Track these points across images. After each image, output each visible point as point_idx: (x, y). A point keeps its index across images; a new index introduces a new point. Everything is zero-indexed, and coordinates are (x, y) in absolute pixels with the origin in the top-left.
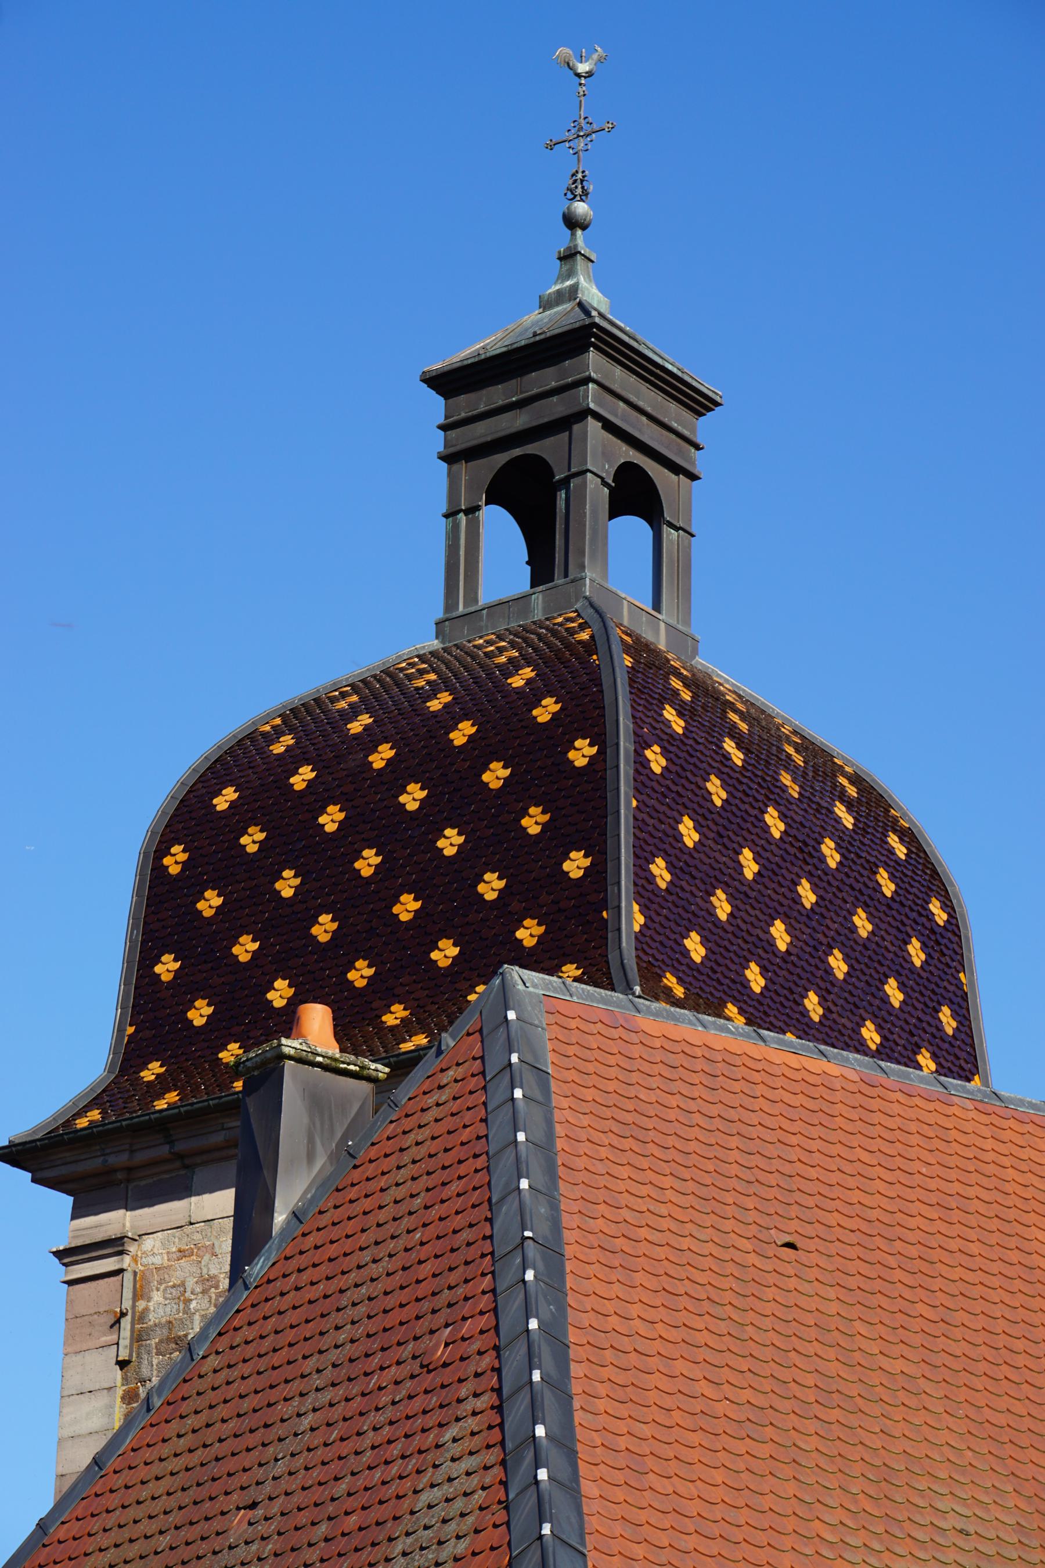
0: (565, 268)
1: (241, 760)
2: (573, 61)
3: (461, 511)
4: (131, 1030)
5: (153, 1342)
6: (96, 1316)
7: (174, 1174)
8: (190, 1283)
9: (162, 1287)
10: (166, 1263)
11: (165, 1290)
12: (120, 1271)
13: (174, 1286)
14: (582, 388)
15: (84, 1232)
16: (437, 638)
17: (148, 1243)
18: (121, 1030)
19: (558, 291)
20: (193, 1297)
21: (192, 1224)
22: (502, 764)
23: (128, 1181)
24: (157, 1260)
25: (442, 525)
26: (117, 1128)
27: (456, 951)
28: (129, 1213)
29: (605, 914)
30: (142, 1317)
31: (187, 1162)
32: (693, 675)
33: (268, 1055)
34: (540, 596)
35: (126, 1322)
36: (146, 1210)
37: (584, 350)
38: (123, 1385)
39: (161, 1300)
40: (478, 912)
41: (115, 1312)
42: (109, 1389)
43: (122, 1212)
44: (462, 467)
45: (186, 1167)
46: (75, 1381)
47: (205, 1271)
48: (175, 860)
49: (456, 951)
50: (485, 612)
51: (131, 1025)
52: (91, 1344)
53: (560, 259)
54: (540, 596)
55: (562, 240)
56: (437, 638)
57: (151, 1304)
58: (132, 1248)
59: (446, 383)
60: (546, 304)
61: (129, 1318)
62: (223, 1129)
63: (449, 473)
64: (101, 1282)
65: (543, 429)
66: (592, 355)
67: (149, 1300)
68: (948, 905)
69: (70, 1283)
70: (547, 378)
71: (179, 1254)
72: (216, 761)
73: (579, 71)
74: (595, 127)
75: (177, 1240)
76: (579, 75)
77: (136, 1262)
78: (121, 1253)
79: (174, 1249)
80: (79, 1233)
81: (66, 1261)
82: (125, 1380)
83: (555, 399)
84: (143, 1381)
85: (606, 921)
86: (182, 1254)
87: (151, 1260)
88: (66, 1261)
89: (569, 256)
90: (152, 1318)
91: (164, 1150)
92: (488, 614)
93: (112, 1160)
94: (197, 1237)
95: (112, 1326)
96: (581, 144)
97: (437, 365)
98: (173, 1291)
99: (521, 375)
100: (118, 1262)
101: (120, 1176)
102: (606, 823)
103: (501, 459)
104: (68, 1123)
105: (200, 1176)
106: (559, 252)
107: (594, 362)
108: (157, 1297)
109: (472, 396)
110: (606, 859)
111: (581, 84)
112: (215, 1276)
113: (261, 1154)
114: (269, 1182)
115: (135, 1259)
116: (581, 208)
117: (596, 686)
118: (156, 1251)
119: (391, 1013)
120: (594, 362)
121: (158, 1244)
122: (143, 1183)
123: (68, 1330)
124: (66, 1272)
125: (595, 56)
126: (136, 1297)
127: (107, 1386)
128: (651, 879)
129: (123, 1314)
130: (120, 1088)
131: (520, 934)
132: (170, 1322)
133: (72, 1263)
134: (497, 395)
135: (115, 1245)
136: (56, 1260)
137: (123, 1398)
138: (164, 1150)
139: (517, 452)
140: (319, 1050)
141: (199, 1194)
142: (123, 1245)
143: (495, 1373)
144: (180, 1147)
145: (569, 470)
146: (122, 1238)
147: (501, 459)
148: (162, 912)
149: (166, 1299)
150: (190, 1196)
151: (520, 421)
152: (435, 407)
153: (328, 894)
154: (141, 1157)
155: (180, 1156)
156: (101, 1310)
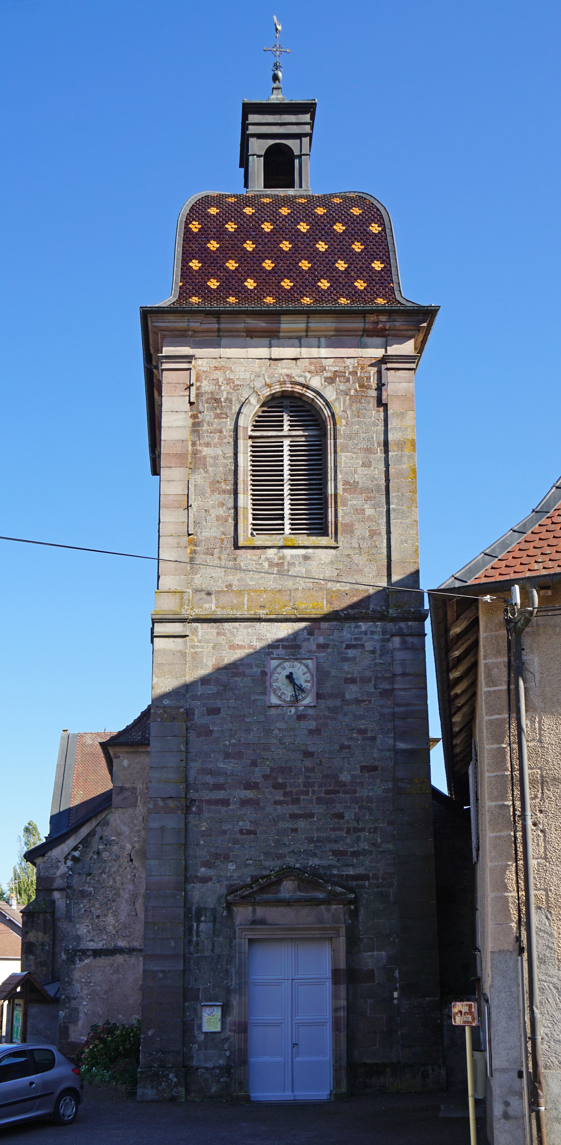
5: (204, 398)
8: (221, 380)
12: (190, 369)
13: (213, 379)
17: (200, 362)
32: (476, 863)
35: (193, 389)
58: (193, 361)
64: (179, 372)
67: (201, 383)
68: (382, 224)
78: (190, 362)
87: (201, 368)
90: (203, 390)
94: (223, 364)
101: (190, 333)
105: (224, 341)
108: (205, 382)
112: (232, 379)
122: (197, 339)
128: (210, 206)
135: (189, 358)
143: (383, 402)
144: (223, 326)
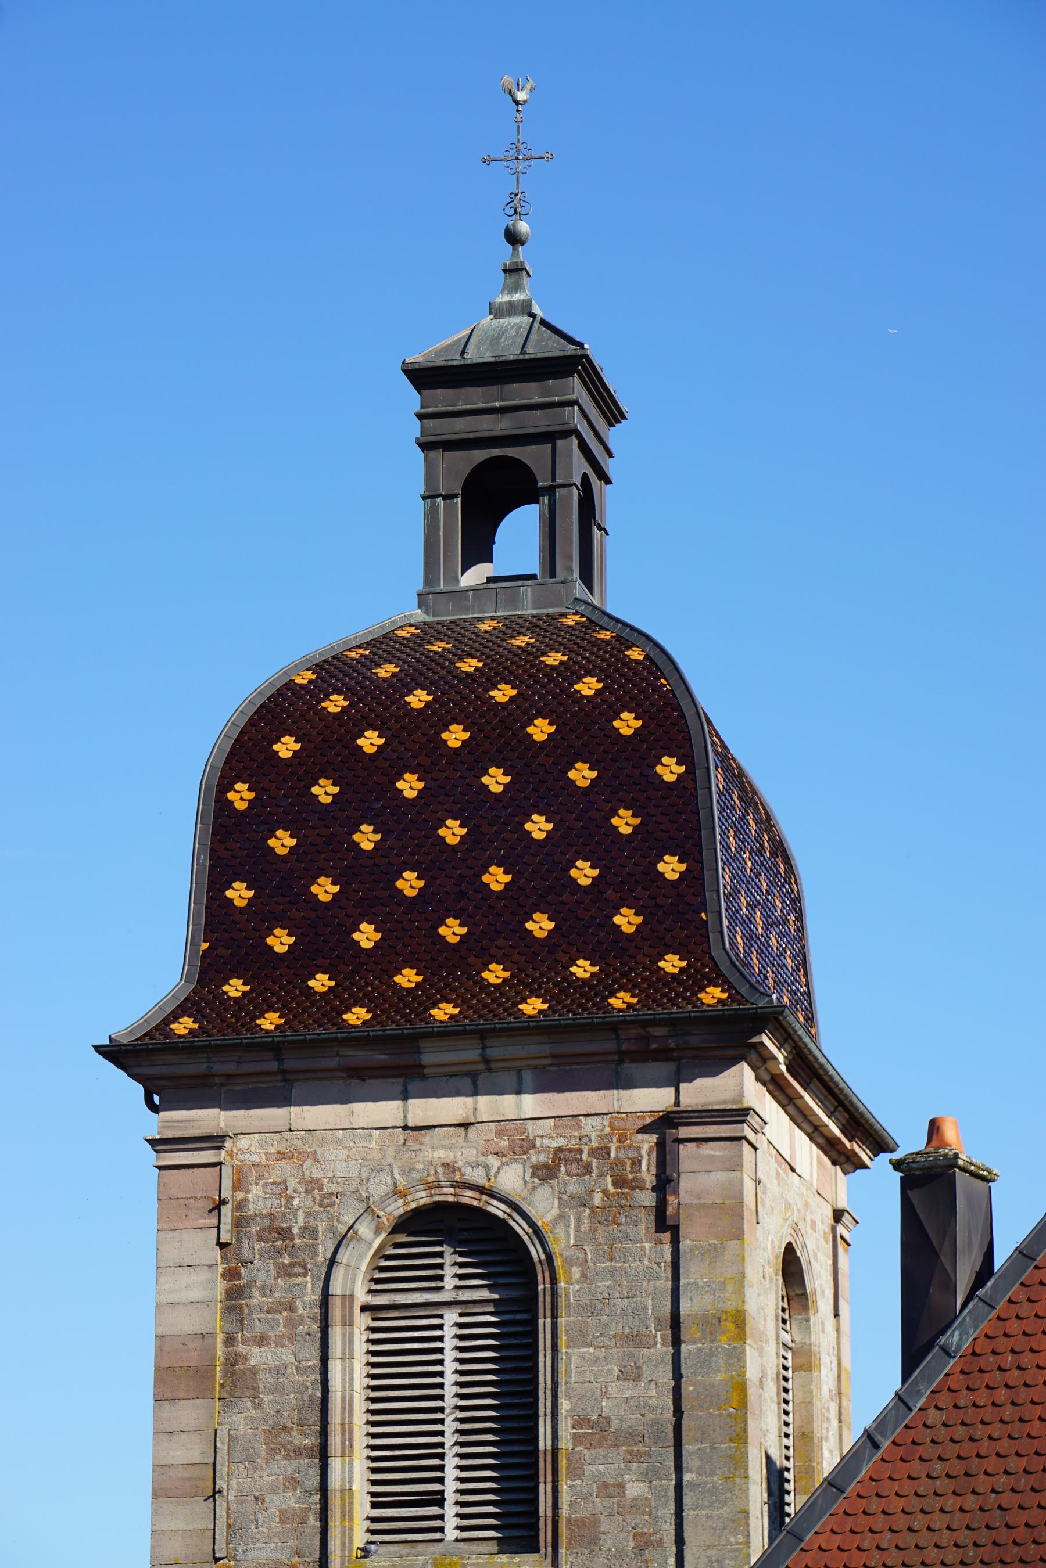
0: (511, 280)
1: (281, 708)
2: (514, 89)
3: (441, 495)
4: (205, 946)
6: (192, 1201)
7: (270, 1085)
8: (292, 1183)
9: (262, 1182)
10: (264, 1162)
11: (265, 1186)
13: (274, 1183)
14: (567, 409)
15: (180, 1124)
16: (419, 607)
17: (244, 1142)
18: (194, 945)
19: (510, 303)
20: (295, 1195)
21: (291, 1130)
22: (588, 765)
23: (222, 1085)
24: (255, 1159)
25: (419, 507)
26: (238, 1044)
27: (551, 925)
28: (222, 1112)
29: (703, 915)
30: (240, 1206)
31: (288, 1076)
33: (940, 1163)
34: (529, 589)
35: (227, 1211)
36: (242, 1112)
37: (570, 374)
38: (222, 1263)
39: (261, 1193)
40: (572, 894)
41: (214, 1200)
42: (211, 1266)
43: (216, 1111)
44: (436, 455)
45: (285, 1080)
46: (172, 1254)
47: (307, 1173)
48: (241, 796)
49: (551, 925)
50: (471, 593)
51: (204, 941)
52: (187, 1224)
53: (505, 271)
54: (529, 589)
55: (505, 253)
56: (419, 607)
57: (250, 1196)
59: (421, 377)
60: (497, 311)
61: (230, 1206)
62: (338, 1055)
63: (426, 459)
65: (510, 433)
66: (576, 380)
67: (248, 1192)
69: (160, 1168)
70: (529, 392)
71: (277, 1156)
72: (261, 706)
73: (519, 99)
74: (534, 154)
75: (275, 1143)
76: (517, 103)
77: (231, 1156)
78: (220, 1148)
79: (273, 1151)
80: (170, 1124)
81: (159, 1148)
82: (225, 1259)
83: (539, 412)
84: (244, 1263)
85: (706, 922)
86: (282, 1156)
87: (247, 1157)
88: (159, 1148)
89: (514, 270)
90: (252, 1209)
91: (274, 1066)
92: (474, 596)
93: (217, 1068)
94: (298, 1143)
95: (210, 1211)
96: (521, 165)
97: (414, 358)
98: (274, 1187)
99: (502, 383)
100: (216, 1155)
101: (217, 1080)
102: (700, 836)
103: (479, 456)
104: (163, 1026)
106: (505, 265)
107: (576, 387)
108: (256, 1191)
109: (450, 392)
110: (702, 868)
111: (518, 111)
112: (318, 1180)
113: (935, 1243)
114: (948, 1268)
115: (230, 1154)
116: (523, 227)
117: (675, 710)
118: (252, 1149)
119: (489, 970)
120: (576, 387)
121: (255, 1144)
122: (237, 1088)
123: (161, 1209)
124: (158, 1159)
125: (528, 86)
126: (235, 1188)
127: (210, 1263)
129: (223, 1202)
130: (200, 996)
131: (617, 920)
132: (271, 1214)
133: (165, 1151)
134: (476, 397)
135: (215, 1141)
136: (149, 1146)
137: (223, 1275)
138: (274, 1066)
139: (496, 452)
140: (974, 1161)
141: (299, 1105)
142: (223, 1142)
144: (288, 1065)
145: (554, 479)
146: (225, 1136)
147: (479, 456)
148: (227, 843)
149: (266, 1193)
150: (290, 1106)
151: (502, 426)
152: (411, 399)
153: (412, 854)
154: (245, 1068)
155: (283, 1072)
156: (199, 1195)
